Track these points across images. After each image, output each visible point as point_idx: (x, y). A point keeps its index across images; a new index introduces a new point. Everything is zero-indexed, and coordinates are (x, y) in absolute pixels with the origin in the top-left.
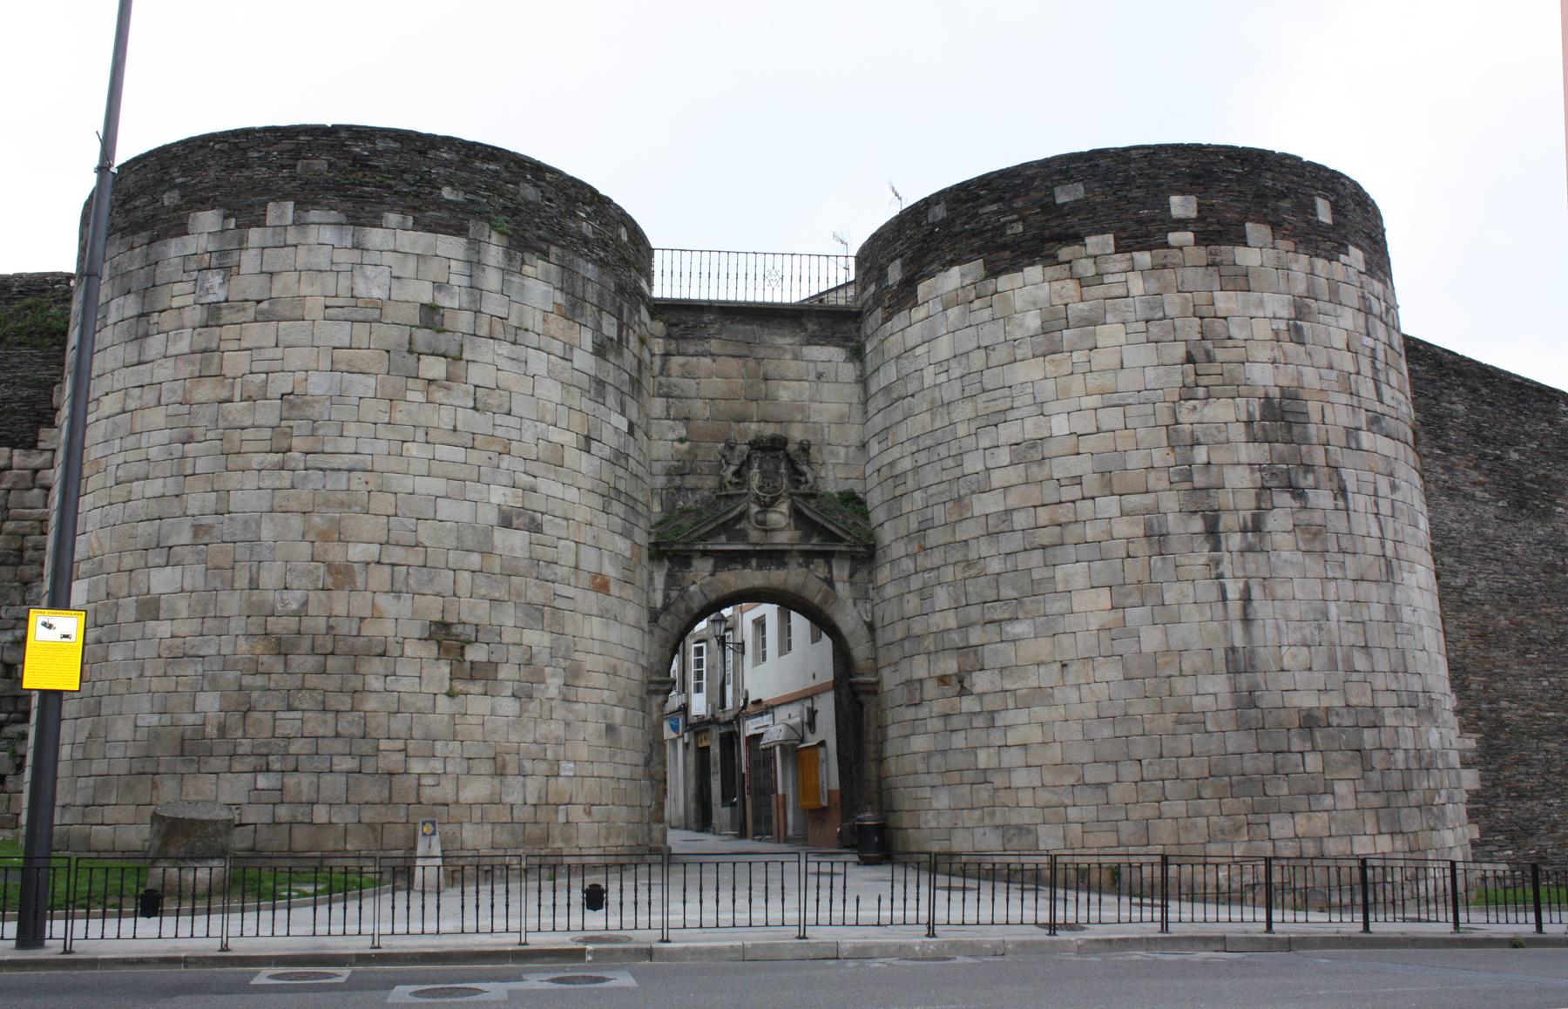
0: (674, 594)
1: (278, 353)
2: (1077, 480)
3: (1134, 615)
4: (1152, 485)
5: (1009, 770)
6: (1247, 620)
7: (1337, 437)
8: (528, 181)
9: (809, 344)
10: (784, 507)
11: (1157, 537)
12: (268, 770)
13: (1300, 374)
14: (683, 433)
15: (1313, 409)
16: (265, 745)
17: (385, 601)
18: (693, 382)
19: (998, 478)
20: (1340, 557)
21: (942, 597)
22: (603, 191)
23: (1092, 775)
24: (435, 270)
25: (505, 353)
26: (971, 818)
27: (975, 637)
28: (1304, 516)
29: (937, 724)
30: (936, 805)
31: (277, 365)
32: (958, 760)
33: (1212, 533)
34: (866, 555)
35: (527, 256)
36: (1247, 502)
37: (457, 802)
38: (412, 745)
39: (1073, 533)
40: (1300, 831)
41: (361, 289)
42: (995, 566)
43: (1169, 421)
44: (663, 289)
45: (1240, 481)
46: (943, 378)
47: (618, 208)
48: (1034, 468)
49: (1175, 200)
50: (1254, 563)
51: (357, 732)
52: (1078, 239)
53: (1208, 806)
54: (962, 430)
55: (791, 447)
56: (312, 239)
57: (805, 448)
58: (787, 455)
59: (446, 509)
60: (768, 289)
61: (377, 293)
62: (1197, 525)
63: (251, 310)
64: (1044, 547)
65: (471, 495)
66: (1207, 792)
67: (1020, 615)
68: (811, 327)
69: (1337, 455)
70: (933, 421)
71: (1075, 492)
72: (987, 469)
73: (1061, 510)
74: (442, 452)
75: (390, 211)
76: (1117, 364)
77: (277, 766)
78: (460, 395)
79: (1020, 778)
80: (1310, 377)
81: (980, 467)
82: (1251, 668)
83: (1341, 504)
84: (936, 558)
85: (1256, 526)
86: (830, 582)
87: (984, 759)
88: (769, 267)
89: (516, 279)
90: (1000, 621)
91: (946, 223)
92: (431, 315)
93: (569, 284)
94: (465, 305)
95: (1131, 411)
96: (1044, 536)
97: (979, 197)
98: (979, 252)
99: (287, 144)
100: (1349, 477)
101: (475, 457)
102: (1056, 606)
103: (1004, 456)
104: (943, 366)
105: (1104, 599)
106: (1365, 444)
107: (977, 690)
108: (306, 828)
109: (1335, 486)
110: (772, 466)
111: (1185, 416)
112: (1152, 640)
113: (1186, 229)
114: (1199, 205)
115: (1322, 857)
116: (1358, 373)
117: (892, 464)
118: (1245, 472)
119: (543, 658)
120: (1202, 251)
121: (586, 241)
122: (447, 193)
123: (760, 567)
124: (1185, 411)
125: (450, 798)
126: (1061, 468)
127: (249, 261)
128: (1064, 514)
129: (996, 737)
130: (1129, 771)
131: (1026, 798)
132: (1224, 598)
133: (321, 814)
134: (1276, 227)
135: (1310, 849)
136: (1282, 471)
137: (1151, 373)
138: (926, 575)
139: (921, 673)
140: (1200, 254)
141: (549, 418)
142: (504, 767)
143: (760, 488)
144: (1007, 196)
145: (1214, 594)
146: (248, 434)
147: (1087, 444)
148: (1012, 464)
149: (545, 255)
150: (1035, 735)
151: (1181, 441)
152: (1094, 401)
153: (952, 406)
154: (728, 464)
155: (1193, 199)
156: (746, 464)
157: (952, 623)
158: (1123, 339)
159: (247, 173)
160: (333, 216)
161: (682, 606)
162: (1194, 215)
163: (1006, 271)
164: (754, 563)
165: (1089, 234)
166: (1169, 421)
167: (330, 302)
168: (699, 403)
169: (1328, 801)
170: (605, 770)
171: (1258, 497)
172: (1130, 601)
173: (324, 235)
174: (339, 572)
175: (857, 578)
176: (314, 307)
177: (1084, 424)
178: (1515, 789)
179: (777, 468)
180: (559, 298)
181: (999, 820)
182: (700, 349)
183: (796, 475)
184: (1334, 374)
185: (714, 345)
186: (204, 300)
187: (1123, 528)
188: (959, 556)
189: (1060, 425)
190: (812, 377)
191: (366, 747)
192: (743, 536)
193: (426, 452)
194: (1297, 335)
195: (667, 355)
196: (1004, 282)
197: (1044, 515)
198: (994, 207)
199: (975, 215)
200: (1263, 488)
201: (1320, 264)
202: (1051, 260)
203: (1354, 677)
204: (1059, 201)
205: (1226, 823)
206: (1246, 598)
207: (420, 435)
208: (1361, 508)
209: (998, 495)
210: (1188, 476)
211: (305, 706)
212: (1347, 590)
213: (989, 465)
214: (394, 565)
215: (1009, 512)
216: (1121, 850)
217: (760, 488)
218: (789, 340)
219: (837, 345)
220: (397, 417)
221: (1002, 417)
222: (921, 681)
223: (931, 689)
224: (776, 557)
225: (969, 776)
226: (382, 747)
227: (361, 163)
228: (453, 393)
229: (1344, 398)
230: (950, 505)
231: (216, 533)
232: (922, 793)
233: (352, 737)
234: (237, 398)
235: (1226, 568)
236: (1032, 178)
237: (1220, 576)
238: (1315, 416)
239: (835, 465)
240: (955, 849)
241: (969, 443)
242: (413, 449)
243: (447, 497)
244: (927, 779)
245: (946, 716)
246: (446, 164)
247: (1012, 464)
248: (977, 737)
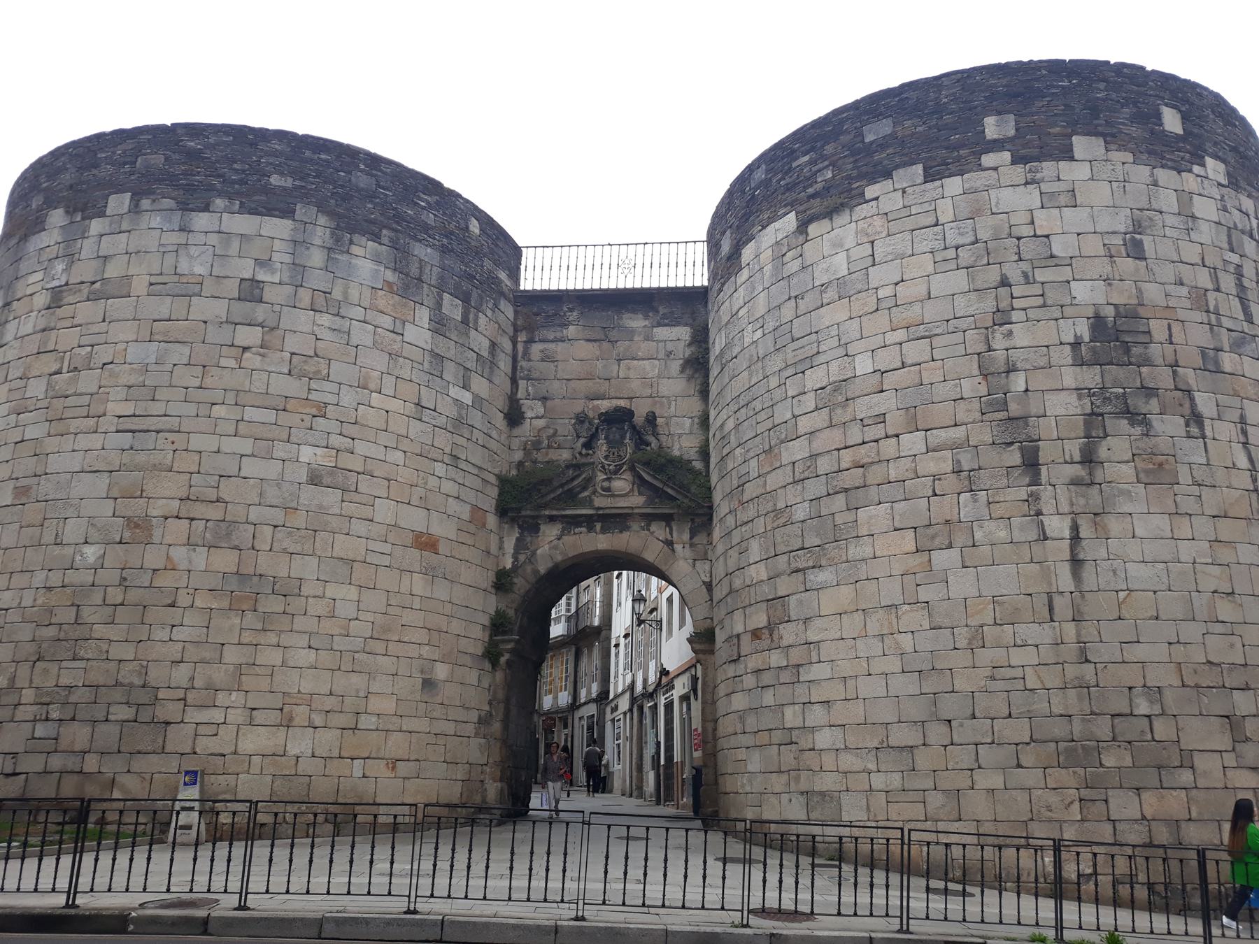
1: (104, 327)
2: (881, 419)
3: (942, 559)
4: (961, 417)
5: (813, 730)
6: (1076, 563)
7: (1191, 356)
8: (362, 171)
9: (659, 325)
12: (47, 719)
13: (1139, 290)
14: (541, 411)
15: (1158, 329)
16: (48, 694)
17: (179, 554)
18: (552, 365)
20: (1195, 490)
22: (448, 183)
23: (900, 736)
24: (257, 250)
25: (326, 324)
26: (778, 783)
28: (1145, 443)
29: (749, 681)
30: (750, 768)
31: (102, 338)
32: (768, 720)
33: (1031, 464)
34: (699, 515)
35: (356, 238)
37: (235, 753)
38: (191, 697)
40: (1149, 813)
41: (184, 267)
43: (981, 347)
44: (530, 280)
47: (467, 201)
48: (839, 411)
51: (137, 681)
53: (1032, 777)
55: (639, 419)
56: (144, 226)
57: (651, 419)
58: (633, 427)
59: (251, 468)
60: (622, 277)
61: (199, 270)
62: (1014, 457)
63: (85, 289)
64: (846, 490)
65: (278, 453)
67: (824, 563)
68: (662, 310)
69: (1189, 376)
70: (750, 380)
71: (878, 431)
72: (795, 417)
73: (863, 450)
74: (250, 413)
75: (219, 196)
76: (925, 293)
77: (55, 715)
78: (278, 361)
79: (824, 739)
80: (1153, 293)
81: (789, 415)
83: (1195, 430)
84: (751, 511)
86: (669, 544)
87: (791, 716)
88: (623, 256)
89: (343, 258)
90: (803, 570)
91: (765, 183)
92: (251, 291)
93: (400, 260)
94: (286, 280)
95: (937, 341)
96: (848, 479)
97: (793, 151)
98: (792, 205)
99: (130, 145)
100: (1205, 403)
101: (284, 418)
102: (854, 551)
104: (760, 322)
106: (1227, 367)
107: (785, 643)
108: (76, 777)
109: (1187, 411)
110: (618, 436)
111: (998, 342)
112: (962, 584)
115: (1180, 846)
116: (1218, 290)
118: (1073, 399)
120: (1019, 169)
121: (426, 228)
122: (275, 180)
123: (603, 531)
124: (998, 336)
125: (227, 750)
126: (863, 408)
127: (87, 248)
128: (864, 453)
129: (801, 693)
130: (937, 733)
131: (828, 761)
133: (91, 763)
135: (1163, 835)
136: (1117, 396)
139: (739, 628)
140: (1019, 173)
141: (372, 386)
142: (291, 719)
143: (606, 457)
144: (819, 144)
146: (70, 401)
147: (890, 381)
148: (817, 409)
149: (376, 238)
151: (996, 373)
152: (900, 335)
153: (766, 361)
154: (578, 437)
157: (764, 576)
158: (930, 269)
159: (95, 172)
160: (167, 203)
161: (529, 568)
162: (1012, 132)
164: (598, 526)
165: (897, 167)
166: (981, 347)
167: (153, 280)
168: (556, 384)
169: (1186, 777)
170: (421, 725)
172: (937, 542)
173: (156, 226)
174: (137, 526)
175: (696, 540)
176: (139, 286)
177: (887, 359)
179: (623, 437)
181: (804, 786)
182: (559, 335)
183: (641, 442)
184: (1184, 291)
185: (571, 331)
186: (49, 286)
187: (930, 465)
188: (770, 507)
190: (661, 355)
191: (143, 697)
192: (589, 502)
193: (235, 413)
194: (1136, 251)
197: (847, 457)
198: (806, 158)
199: (790, 169)
200: (1093, 414)
201: (1163, 175)
207: (230, 398)
208: (1224, 436)
209: (803, 441)
210: (1004, 406)
211: (90, 656)
212: (1204, 527)
213: (796, 413)
214: (192, 519)
216: (929, 825)
220: (208, 382)
221: (807, 364)
222: (738, 636)
223: (747, 645)
224: (614, 521)
225: (777, 736)
226: (160, 696)
227: (192, 155)
228: (267, 360)
229: (1199, 316)
230: (762, 457)
231: (33, 493)
233: (131, 685)
234: (65, 370)
235: (1047, 506)
236: (842, 122)
237: (1039, 513)
239: (680, 435)
240: (765, 817)
242: (218, 411)
243: (253, 455)
245: (758, 671)
246: (275, 154)
247: (817, 409)
248: (784, 693)
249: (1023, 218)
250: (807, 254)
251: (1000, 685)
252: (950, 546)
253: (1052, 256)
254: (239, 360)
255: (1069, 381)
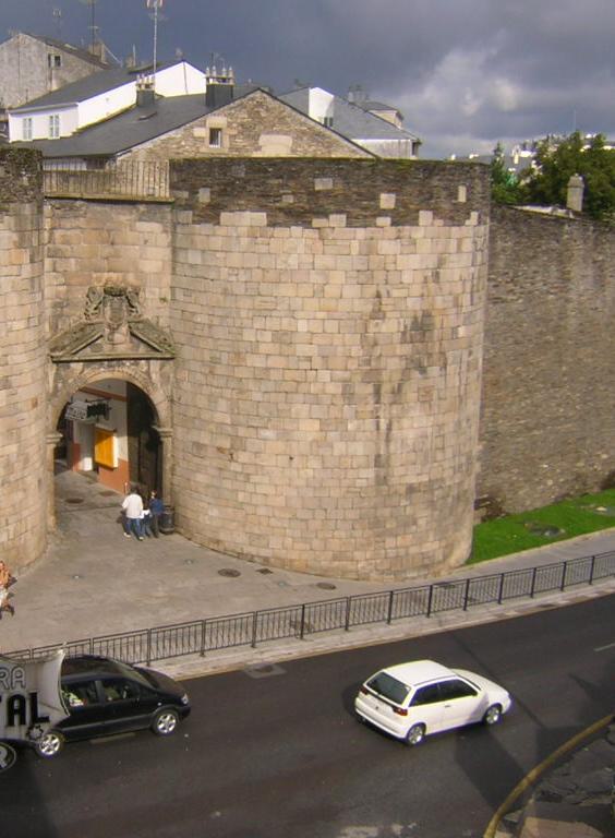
0: (60, 385)
2: (309, 359)
3: (332, 435)
5: (256, 506)
6: (388, 440)
9: (140, 220)
10: (124, 329)
11: (348, 395)
18: (68, 247)
19: (263, 348)
21: (223, 405)
23: (301, 514)
27: (242, 432)
33: (377, 392)
36: (397, 377)
39: (303, 388)
42: (257, 396)
45: (393, 365)
46: (234, 278)
48: (285, 347)
49: (383, 196)
50: (395, 410)
52: (325, 215)
54: (243, 314)
62: (370, 389)
66: (357, 527)
82: (388, 465)
85: (398, 392)
87: (241, 497)
90: (257, 428)
97: (267, 172)
100: (450, 355)
103: (268, 336)
105: (317, 425)
111: (372, 329)
112: (339, 448)
113: (386, 216)
114: (397, 200)
117: (194, 314)
119: (13, 459)
120: (394, 229)
129: (250, 487)
130: (320, 515)
132: (378, 428)
134: (437, 213)
137: (357, 302)
138: (214, 389)
139: (206, 441)
145: (373, 427)
150: (270, 490)
152: (322, 315)
155: (393, 196)
156: (103, 302)
161: (65, 392)
163: (280, 225)
165: (332, 213)
169: (414, 528)
171: (403, 374)
172: (330, 428)
177: (316, 327)
178: (497, 468)
179: (121, 306)
180: (15, 237)
181: (247, 529)
185: (81, 222)
189: (302, 326)
194: (436, 276)
195: (53, 229)
196: (278, 231)
198: (276, 182)
202: (308, 225)
203: (436, 464)
204: (317, 188)
205: (364, 542)
206: (389, 428)
215: (267, 369)
217: (111, 319)
218: (128, 217)
219: (157, 222)
223: (211, 452)
232: (202, 504)
235: (381, 414)
238: (438, 325)
241: (247, 322)
244: (208, 499)
249: (390, 259)
250: (272, 245)
251: (350, 495)
252: (336, 430)
253: (401, 283)
254: (282, 472)
255: (398, 352)
